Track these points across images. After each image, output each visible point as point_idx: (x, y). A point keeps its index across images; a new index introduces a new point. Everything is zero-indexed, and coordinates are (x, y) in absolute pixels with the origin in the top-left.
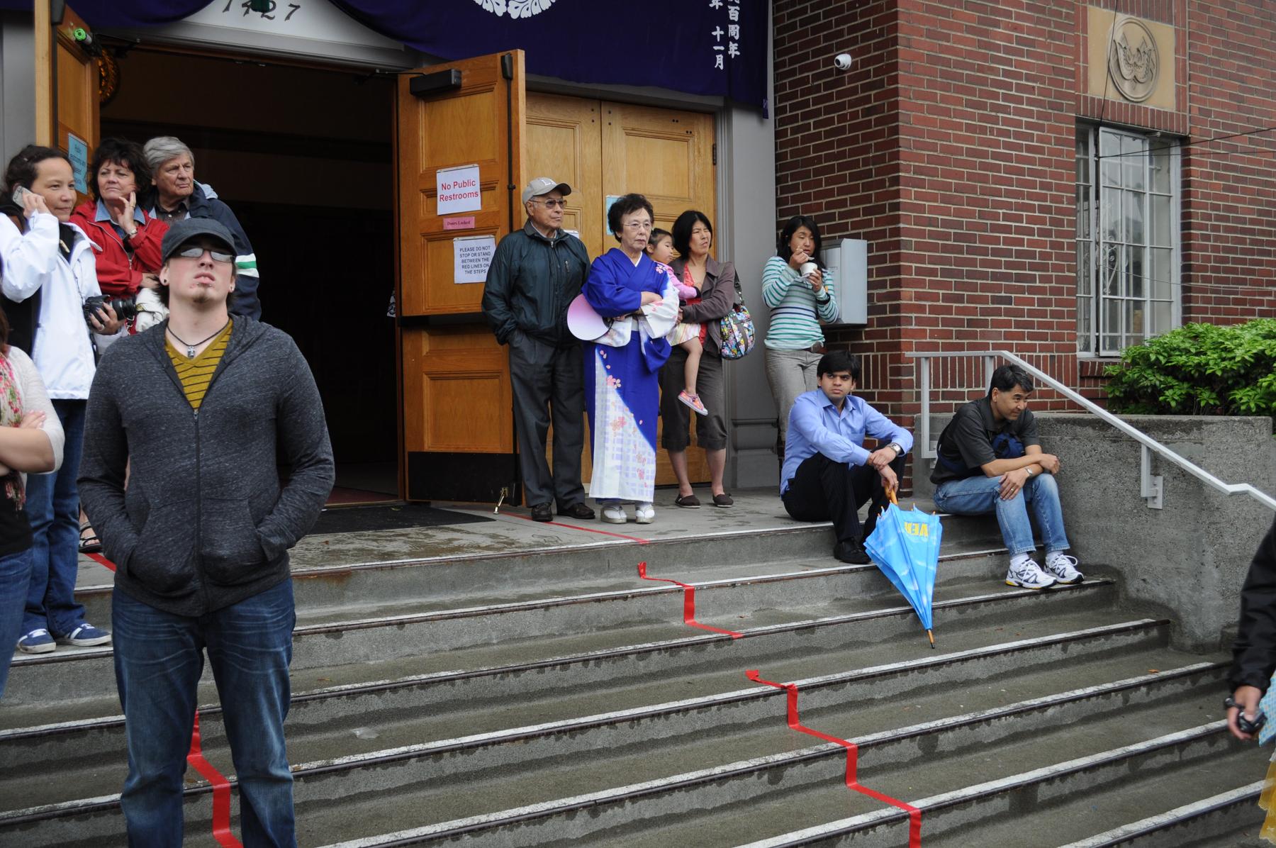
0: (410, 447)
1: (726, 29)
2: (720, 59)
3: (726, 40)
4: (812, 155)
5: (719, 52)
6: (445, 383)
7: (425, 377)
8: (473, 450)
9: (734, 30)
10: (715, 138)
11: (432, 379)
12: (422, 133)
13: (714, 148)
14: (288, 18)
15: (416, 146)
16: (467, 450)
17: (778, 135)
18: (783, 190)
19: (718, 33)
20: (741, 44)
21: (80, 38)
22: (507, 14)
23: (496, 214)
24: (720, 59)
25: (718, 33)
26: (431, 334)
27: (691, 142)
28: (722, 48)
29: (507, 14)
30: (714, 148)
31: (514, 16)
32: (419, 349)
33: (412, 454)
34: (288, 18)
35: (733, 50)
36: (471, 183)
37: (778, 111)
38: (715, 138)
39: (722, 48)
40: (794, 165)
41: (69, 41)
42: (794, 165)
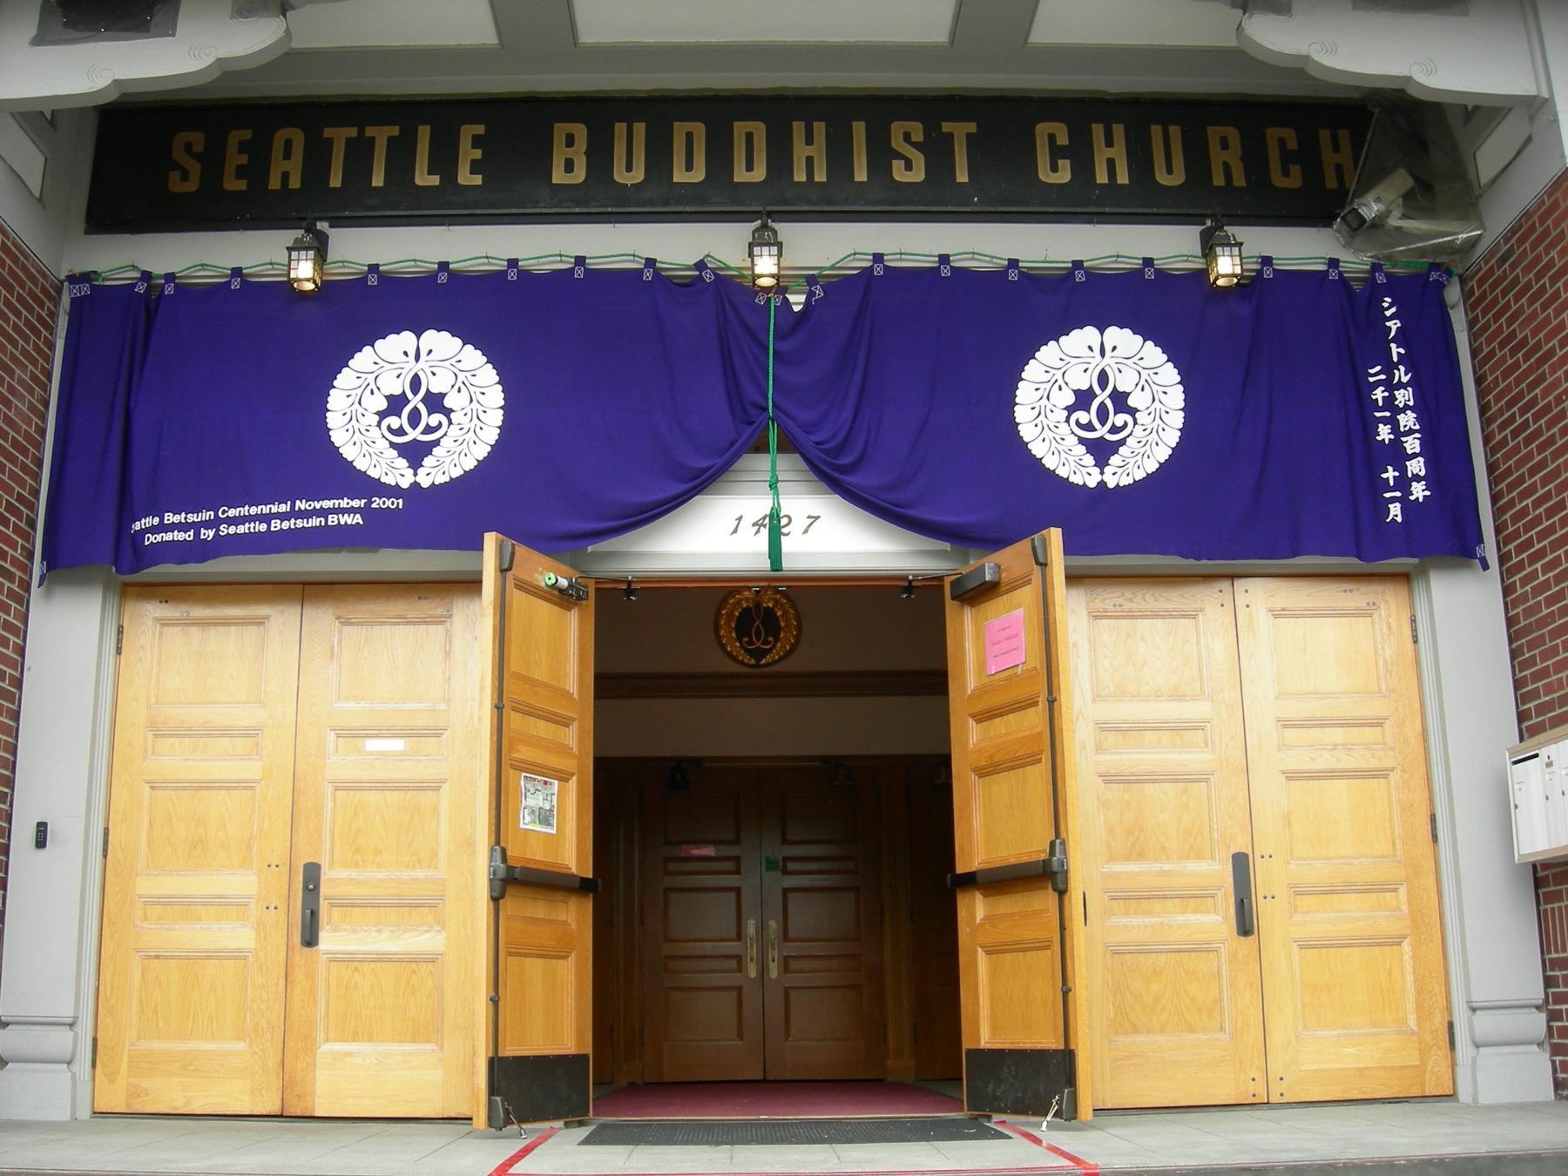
0: (966, 1044)
1: (1402, 469)
2: (1395, 510)
3: (1404, 483)
4: (1545, 612)
5: (1393, 500)
6: (1001, 956)
7: (981, 955)
8: (1029, 1046)
9: (1416, 466)
10: (1412, 607)
11: (988, 953)
12: (969, 645)
13: (1413, 621)
14: (806, 531)
15: (963, 661)
16: (1022, 1046)
17: (1507, 591)
18: (1524, 665)
19: (1390, 474)
20: (1431, 479)
21: (550, 583)
22: (1102, 484)
23: (1040, 734)
24: (1395, 510)
25: (1390, 474)
26: (985, 896)
27: (1376, 616)
28: (1398, 494)
29: (1102, 484)
30: (1413, 621)
31: (1111, 485)
32: (972, 915)
33: (969, 1051)
34: (806, 531)
35: (1419, 491)
36: (563, 750)
37: (1503, 559)
38: (1412, 607)
39: (1398, 494)
40: (1527, 630)
41: (538, 588)
42: (1527, 630)
